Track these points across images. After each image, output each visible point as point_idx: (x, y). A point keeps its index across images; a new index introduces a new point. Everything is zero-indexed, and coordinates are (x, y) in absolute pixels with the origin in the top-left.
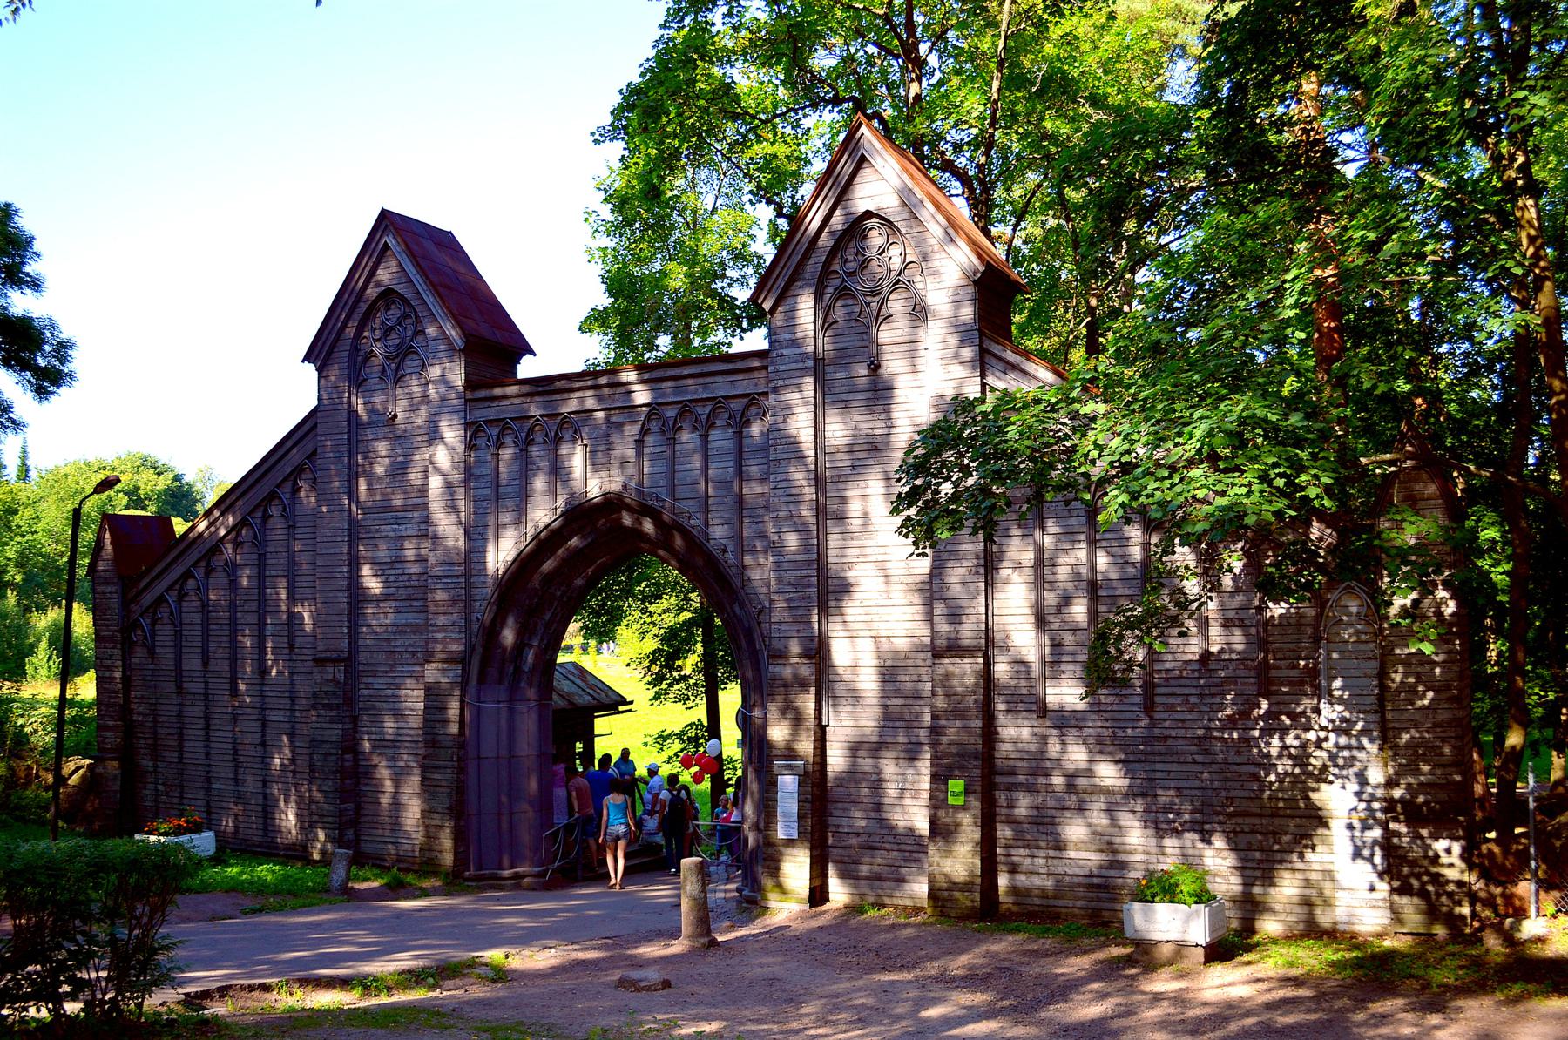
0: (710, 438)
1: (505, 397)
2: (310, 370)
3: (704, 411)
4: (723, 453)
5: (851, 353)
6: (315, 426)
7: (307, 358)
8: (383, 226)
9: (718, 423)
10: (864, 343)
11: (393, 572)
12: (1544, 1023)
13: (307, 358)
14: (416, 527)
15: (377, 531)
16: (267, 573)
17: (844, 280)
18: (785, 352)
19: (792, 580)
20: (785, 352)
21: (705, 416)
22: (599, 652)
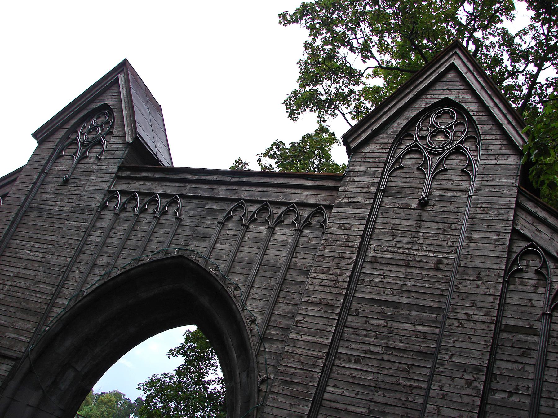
0: (275, 232)
1: (144, 190)
2: (34, 144)
3: (277, 211)
4: (283, 245)
5: (408, 191)
6: (15, 180)
7: (35, 135)
8: (121, 69)
9: (286, 222)
10: (420, 186)
11: (9, 283)
12: (283, 397)
13: (35, 135)
14: (41, 255)
15: (16, 253)
16: (508, 301)
17: (416, 141)
18: (357, 179)
20: (357, 179)
21: (277, 216)
22: (287, 112)
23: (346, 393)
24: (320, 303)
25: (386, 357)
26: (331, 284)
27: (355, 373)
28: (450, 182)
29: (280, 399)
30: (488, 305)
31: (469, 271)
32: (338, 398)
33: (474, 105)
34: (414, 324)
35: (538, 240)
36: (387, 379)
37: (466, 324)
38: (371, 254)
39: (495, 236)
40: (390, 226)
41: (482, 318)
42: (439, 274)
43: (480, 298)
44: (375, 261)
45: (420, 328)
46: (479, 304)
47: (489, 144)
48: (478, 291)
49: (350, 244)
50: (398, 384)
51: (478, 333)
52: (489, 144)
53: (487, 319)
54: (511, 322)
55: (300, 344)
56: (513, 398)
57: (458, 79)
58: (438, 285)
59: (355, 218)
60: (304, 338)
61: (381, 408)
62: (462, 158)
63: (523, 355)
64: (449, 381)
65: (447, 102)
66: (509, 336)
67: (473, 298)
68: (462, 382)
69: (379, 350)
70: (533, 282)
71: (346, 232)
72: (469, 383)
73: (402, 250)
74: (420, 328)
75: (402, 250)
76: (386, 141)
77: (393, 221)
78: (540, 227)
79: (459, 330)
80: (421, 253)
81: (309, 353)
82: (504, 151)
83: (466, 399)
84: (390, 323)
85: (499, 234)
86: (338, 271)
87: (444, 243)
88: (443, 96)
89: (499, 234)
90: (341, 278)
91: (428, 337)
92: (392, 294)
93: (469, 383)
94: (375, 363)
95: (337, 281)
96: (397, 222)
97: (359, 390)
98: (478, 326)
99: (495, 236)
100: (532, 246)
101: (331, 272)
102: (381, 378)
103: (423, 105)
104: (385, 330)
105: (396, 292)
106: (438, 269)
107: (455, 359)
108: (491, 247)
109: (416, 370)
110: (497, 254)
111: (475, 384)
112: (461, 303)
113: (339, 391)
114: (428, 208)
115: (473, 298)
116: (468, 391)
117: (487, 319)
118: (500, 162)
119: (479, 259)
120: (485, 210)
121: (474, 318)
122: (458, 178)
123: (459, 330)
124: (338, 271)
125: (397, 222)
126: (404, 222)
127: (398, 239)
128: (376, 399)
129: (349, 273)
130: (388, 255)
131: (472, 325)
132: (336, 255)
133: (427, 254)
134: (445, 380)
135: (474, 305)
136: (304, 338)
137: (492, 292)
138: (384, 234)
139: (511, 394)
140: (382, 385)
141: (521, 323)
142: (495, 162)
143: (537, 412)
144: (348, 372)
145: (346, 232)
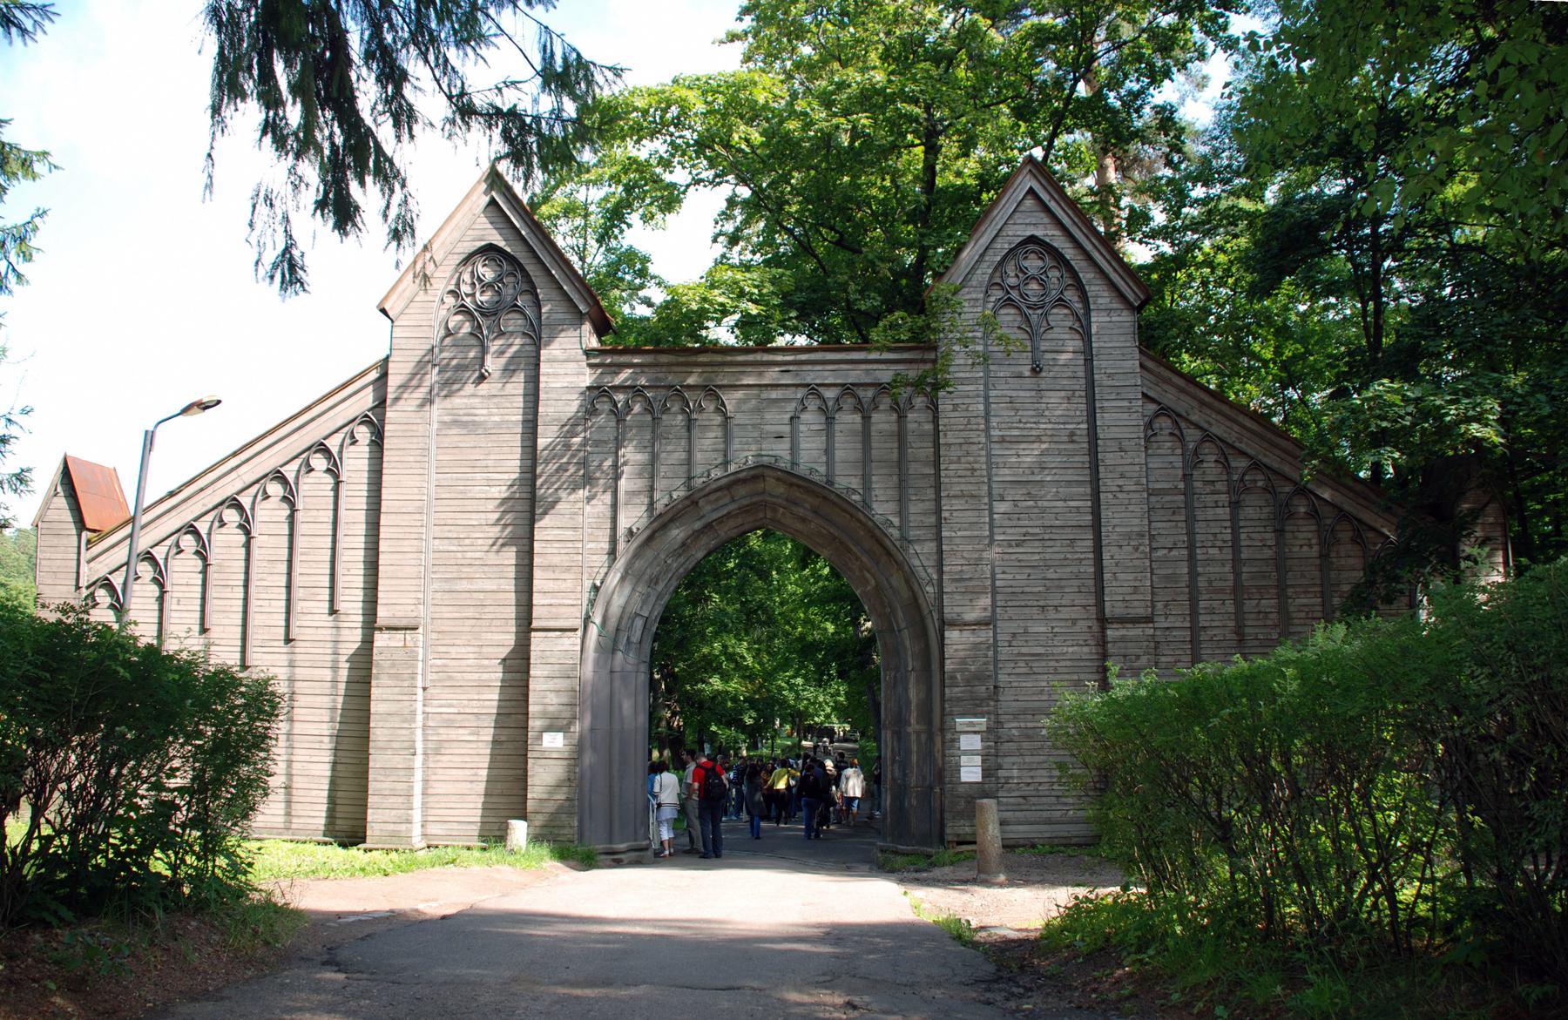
0: (873, 420)
23: (1018, 577)
24: (963, 496)
25: (1047, 537)
26: (969, 473)
27: (1021, 557)
28: (1060, 343)
29: (958, 597)
30: (1137, 475)
31: (1109, 443)
32: (1010, 583)
33: (1106, 294)
34: (1065, 501)
35: (1165, 401)
36: (1053, 556)
37: (1119, 495)
38: (996, 433)
39: (1126, 404)
40: (1008, 400)
41: (1133, 488)
42: (1076, 446)
43: (1126, 468)
44: (1002, 440)
45: (1072, 504)
46: (1128, 475)
47: (1097, 296)
48: (1123, 462)
49: (975, 427)
50: (1066, 559)
51: (1133, 501)
52: (1097, 296)
53: (1139, 488)
54: (1158, 486)
55: (958, 541)
56: (1173, 553)
57: (1070, 245)
58: (1077, 459)
59: (968, 397)
60: (959, 534)
61: (1056, 583)
62: (1066, 311)
63: (1174, 513)
64: (1116, 549)
65: (1032, 239)
66: (1159, 498)
67: (1120, 469)
68: (1130, 548)
69: (1037, 530)
70: (1169, 444)
71: (963, 414)
72: (1136, 549)
73: (1028, 425)
74: (1072, 504)
75: (1028, 425)
76: (974, 296)
77: (1009, 393)
78: (1166, 387)
79: (1115, 502)
80: (1050, 426)
81: (970, 548)
82: (1115, 306)
83: (1137, 563)
84: (1040, 503)
85: (1130, 400)
86: (971, 459)
87: (1072, 413)
88: (1028, 233)
89: (1130, 400)
90: (976, 466)
91: (1082, 510)
92: (1033, 473)
93: (1136, 549)
94: (1037, 544)
95: (974, 470)
96: (1014, 394)
97: (1028, 571)
98: (1132, 495)
99: (1126, 404)
100: (1162, 409)
101: (963, 460)
102: (1047, 557)
103: (1006, 246)
104: (1036, 511)
105: (1036, 471)
106: (1072, 442)
107: (1117, 529)
108: (1126, 416)
109: (1079, 543)
110: (1134, 423)
111: (1141, 548)
112: (1110, 476)
113: (1011, 577)
114: (1043, 374)
115: (1120, 469)
116: (1137, 555)
117: (1139, 488)
118: (1114, 319)
119: (1116, 429)
120: (1110, 376)
121: (1126, 488)
122: (1067, 336)
123: (1115, 502)
124: (971, 459)
125: (1014, 394)
126: (1022, 394)
127: (1020, 413)
128: (1049, 576)
129: (983, 459)
130: (1016, 432)
131: (1124, 495)
132: (962, 441)
133: (1056, 426)
134: (1114, 550)
135: (1122, 476)
136: (959, 534)
137: (1137, 461)
138: (1003, 409)
139: (1171, 549)
140: (1049, 563)
141: (1166, 486)
143: (759, 357)
144: (1013, 557)
145: (963, 414)
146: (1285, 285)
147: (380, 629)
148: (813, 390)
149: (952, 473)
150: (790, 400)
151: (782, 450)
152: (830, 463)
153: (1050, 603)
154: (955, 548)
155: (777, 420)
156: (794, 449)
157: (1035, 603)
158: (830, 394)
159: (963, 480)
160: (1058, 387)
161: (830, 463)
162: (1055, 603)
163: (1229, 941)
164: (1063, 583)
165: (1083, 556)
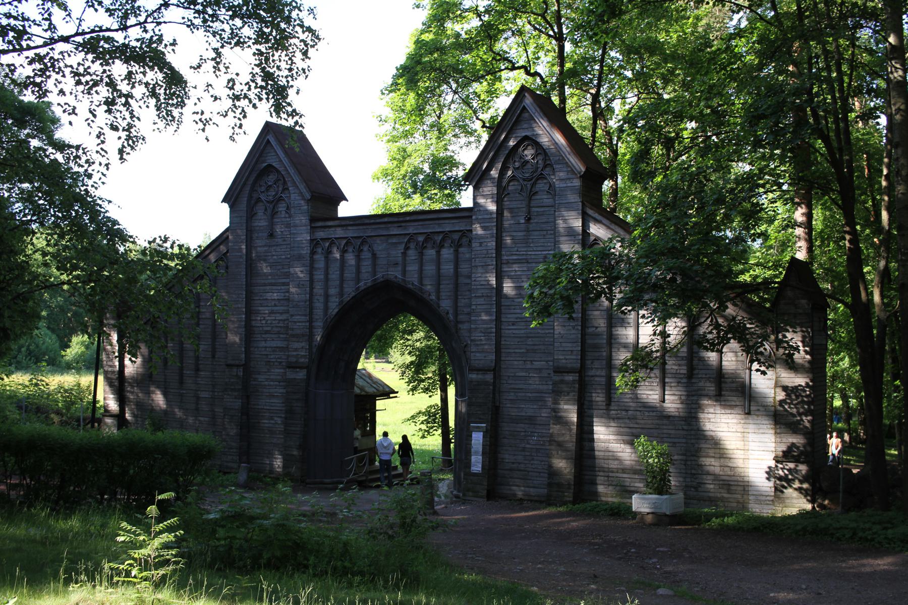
19: (482, 330)
49: (490, 256)
88: (524, 134)
94: (523, 324)
122: (545, 197)
130: (515, 257)
132: (483, 264)
142: (565, 185)
145: (484, 248)
146: (566, 90)
147: (303, 335)
148: (412, 237)
149: (477, 283)
150: (400, 243)
151: (395, 274)
152: (421, 279)
153: (529, 359)
154: (478, 326)
155: (398, 252)
156: (404, 272)
157: (520, 359)
158: (421, 239)
159: (483, 287)
160: (538, 229)
161: (421, 279)
162: (531, 359)
163: (742, 101)
164: (536, 347)
165: (547, 331)
